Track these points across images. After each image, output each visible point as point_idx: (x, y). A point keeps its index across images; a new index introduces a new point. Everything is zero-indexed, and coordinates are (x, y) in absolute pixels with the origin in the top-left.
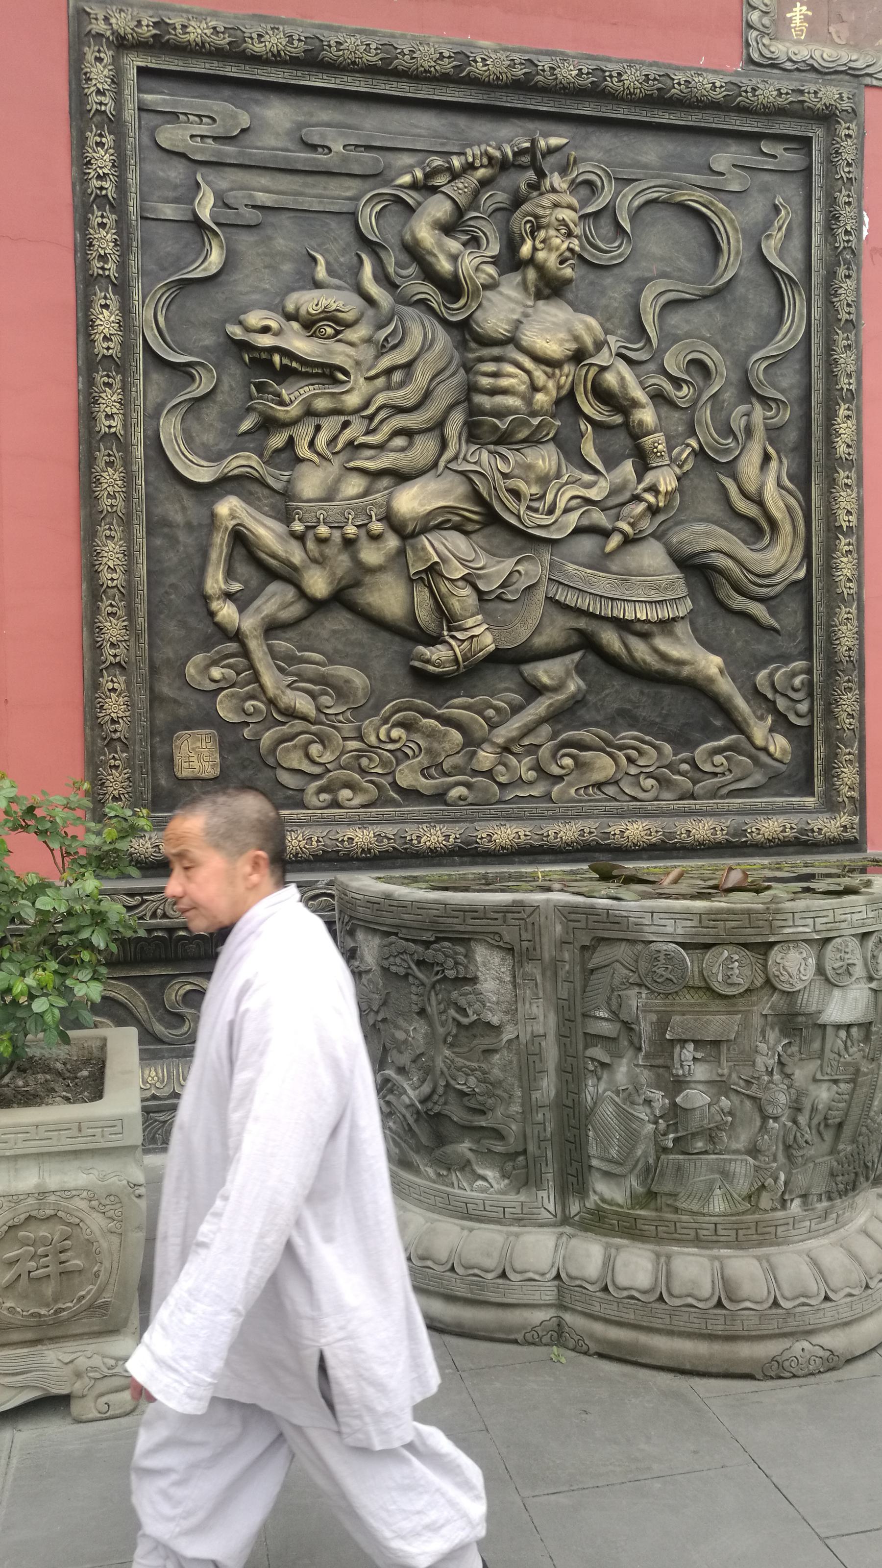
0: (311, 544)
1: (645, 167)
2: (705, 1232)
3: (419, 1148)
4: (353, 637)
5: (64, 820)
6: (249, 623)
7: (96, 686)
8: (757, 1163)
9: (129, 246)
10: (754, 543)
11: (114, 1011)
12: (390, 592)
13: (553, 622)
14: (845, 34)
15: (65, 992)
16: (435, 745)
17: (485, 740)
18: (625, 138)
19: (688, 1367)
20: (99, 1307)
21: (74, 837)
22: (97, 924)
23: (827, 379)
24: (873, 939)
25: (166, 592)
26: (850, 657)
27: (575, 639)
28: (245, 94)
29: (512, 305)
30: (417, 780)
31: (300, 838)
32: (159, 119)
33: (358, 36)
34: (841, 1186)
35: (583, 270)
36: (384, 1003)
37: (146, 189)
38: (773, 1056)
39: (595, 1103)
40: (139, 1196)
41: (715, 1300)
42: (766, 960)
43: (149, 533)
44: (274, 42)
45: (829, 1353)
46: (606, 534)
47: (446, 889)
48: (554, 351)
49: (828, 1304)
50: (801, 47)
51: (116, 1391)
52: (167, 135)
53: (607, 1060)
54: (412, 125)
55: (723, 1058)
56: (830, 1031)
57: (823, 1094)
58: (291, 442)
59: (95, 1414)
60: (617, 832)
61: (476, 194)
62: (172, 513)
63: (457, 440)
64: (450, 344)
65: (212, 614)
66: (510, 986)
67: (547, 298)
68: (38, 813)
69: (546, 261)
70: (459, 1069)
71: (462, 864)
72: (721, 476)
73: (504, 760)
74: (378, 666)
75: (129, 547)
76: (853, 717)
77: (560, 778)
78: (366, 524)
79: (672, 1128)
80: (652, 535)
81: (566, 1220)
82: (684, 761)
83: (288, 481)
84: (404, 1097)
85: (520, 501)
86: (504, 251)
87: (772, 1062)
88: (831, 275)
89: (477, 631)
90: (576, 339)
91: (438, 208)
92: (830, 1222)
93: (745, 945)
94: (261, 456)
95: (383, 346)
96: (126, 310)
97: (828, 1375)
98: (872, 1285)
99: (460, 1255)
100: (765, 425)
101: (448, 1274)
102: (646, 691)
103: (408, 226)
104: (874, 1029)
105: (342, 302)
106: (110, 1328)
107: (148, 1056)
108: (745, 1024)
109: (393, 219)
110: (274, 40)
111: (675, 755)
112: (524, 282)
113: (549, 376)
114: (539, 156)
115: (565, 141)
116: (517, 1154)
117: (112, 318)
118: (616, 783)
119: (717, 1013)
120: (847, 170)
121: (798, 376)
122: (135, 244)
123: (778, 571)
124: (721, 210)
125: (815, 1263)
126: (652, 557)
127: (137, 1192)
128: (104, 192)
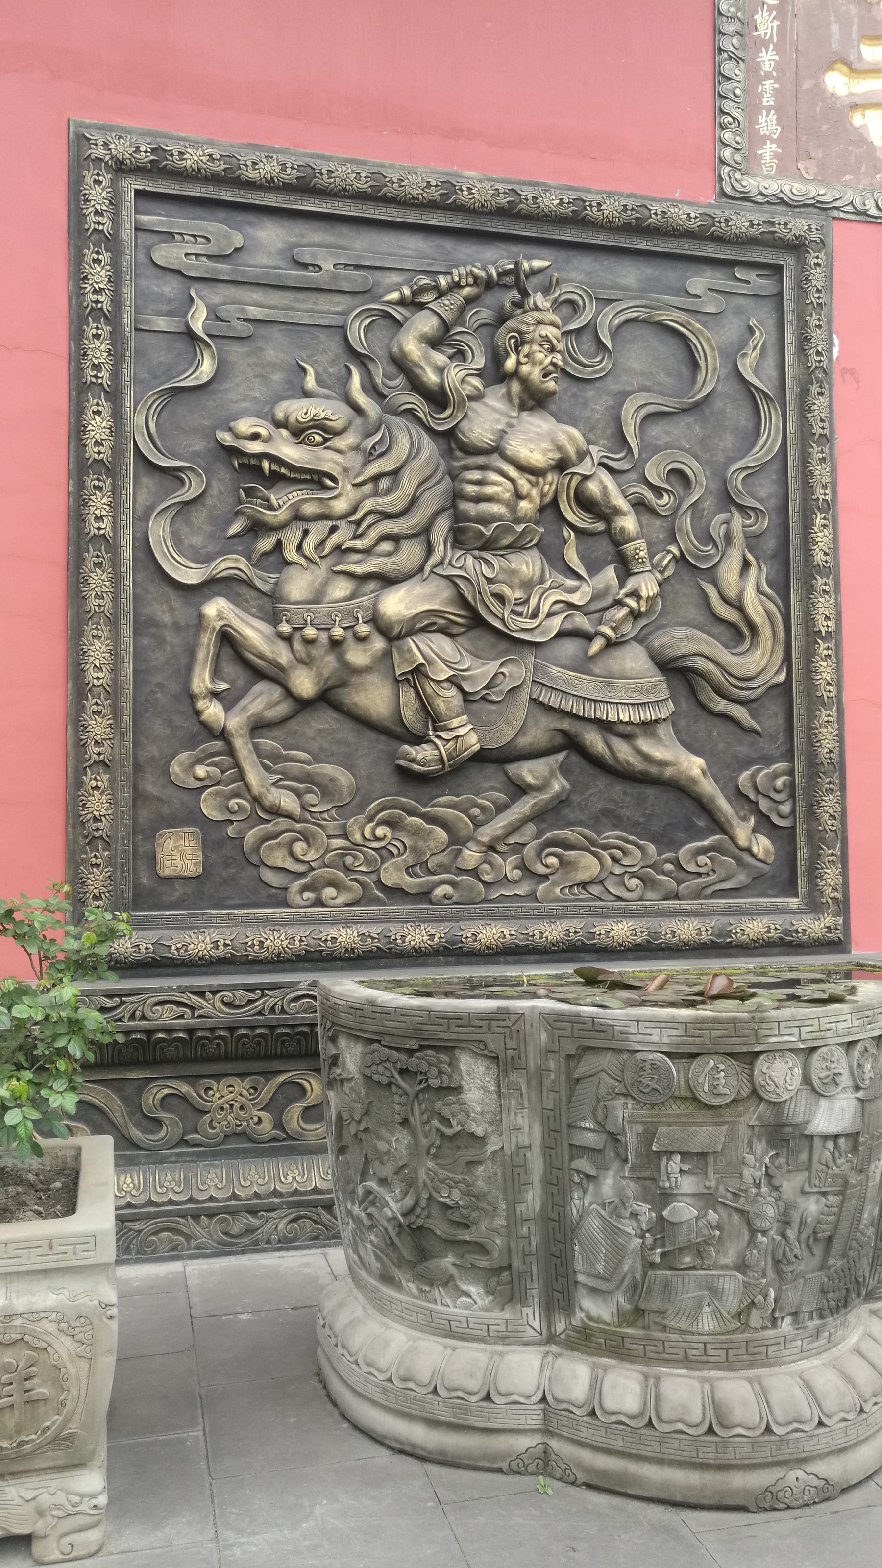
0: (297, 645)
1: (625, 288)
2: (695, 1352)
3: (401, 1263)
4: (339, 736)
5: (42, 924)
6: (235, 722)
7: (79, 784)
8: (746, 1279)
9: (123, 356)
10: (735, 647)
11: (92, 1117)
12: (376, 693)
13: (536, 723)
14: (813, 169)
15: (38, 1103)
16: (421, 843)
17: (470, 839)
18: (606, 262)
19: (679, 1498)
20: (65, 1439)
21: (53, 941)
22: (74, 1032)
23: (804, 489)
24: (859, 1047)
25: (152, 691)
26: (830, 759)
27: (559, 740)
28: (240, 217)
29: (497, 416)
30: (401, 879)
31: (283, 937)
32: (156, 238)
33: (349, 165)
34: (833, 1304)
35: (565, 383)
36: (367, 1113)
37: (140, 302)
38: (760, 1168)
39: (581, 1216)
40: (111, 1317)
41: (706, 1426)
42: (752, 1070)
43: (137, 632)
44: (268, 169)
45: (824, 1482)
46: (589, 637)
47: (428, 994)
48: (537, 460)
49: (822, 1430)
50: (771, 182)
51: (81, 1531)
52: (163, 253)
53: (593, 1172)
54: (401, 247)
55: (710, 1171)
56: (817, 1142)
57: (812, 1207)
58: (279, 545)
59: (57, 1556)
60: (603, 932)
61: (462, 311)
62: (159, 614)
63: (442, 545)
64: (436, 453)
65: (198, 713)
66: (495, 1096)
67: (531, 409)
68: (17, 916)
69: (530, 374)
70: (442, 1182)
71: (447, 964)
72: (702, 583)
73: (489, 858)
74: (363, 764)
75: (115, 647)
76: (834, 818)
77: (546, 877)
78: (353, 627)
79: (659, 1242)
80: (634, 639)
81: (551, 1339)
82: (668, 861)
83: (276, 584)
84: (386, 1210)
85: (504, 604)
86: (489, 364)
87: (760, 1174)
88: (804, 393)
89: (462, 731)
90: (560, 448)
91: (425, 323)
92: (822, 1341)
93: (731, 1055)
94: (249, 559)
95: (371, 454)
96: (117, 416)
97: (823, 1506)
98: (866, 1409)
99: (443, 1376)
100: (744, 532)
101: (430, 1396)
102: (629, 791)
103: (395, 340)
104: (862, 1139)
105: (331, 410)
106: (76, 1461)
107: (123, 1163)
108: (732, 1135)
109: (381, 333)
110: (268, 168)
111: (659, 855)
112: (509, 395)
113: (534, 485)
114: (523, 277)
115: (547, 263)
116: (501, 1269)
117: (104, 424)
118: (601, 882)
119: (704, 1124)
120: (817, 295)
121: (775, 487)
122: (128, 354)
123: (759, 674)
124: (698, 329)
125: (808, 1386)
126: (634, 660)
127: (109, 1313)
128: (99, 306)
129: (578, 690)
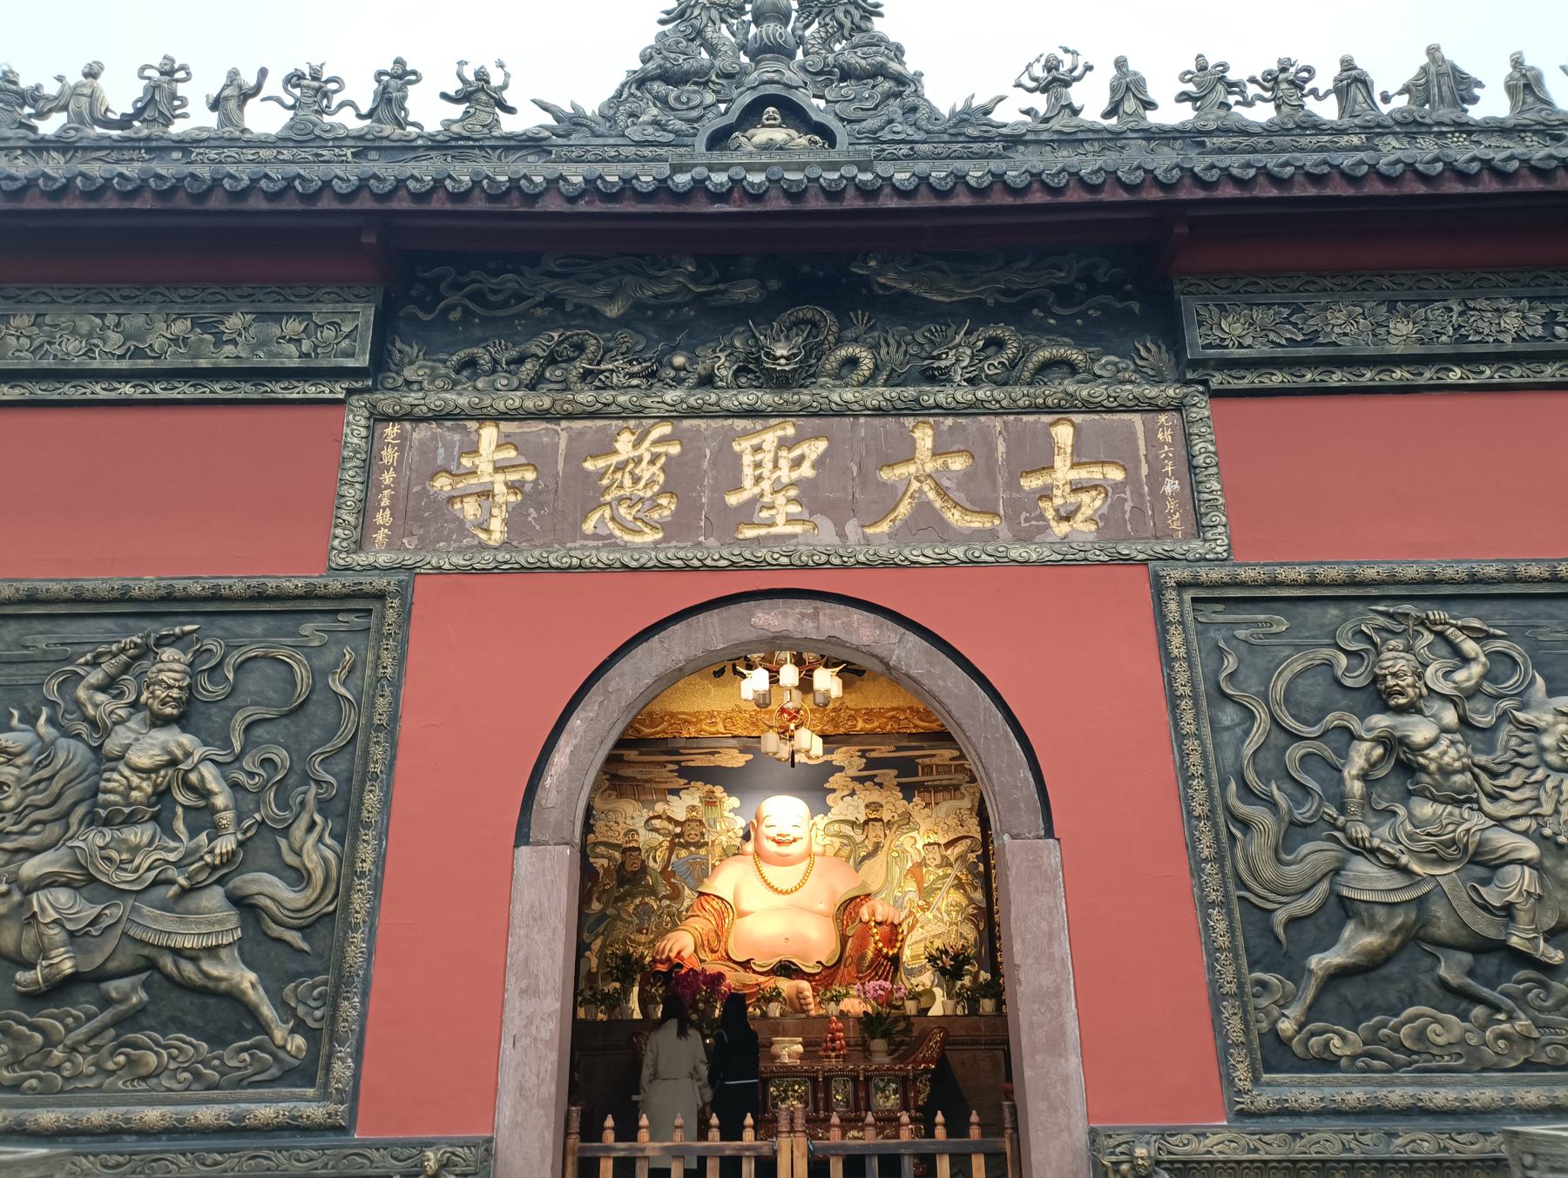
82: (216, 1058)
90: (169, 753)
91: (96, 676)
126: (214, 898)
129: (156, 924)
